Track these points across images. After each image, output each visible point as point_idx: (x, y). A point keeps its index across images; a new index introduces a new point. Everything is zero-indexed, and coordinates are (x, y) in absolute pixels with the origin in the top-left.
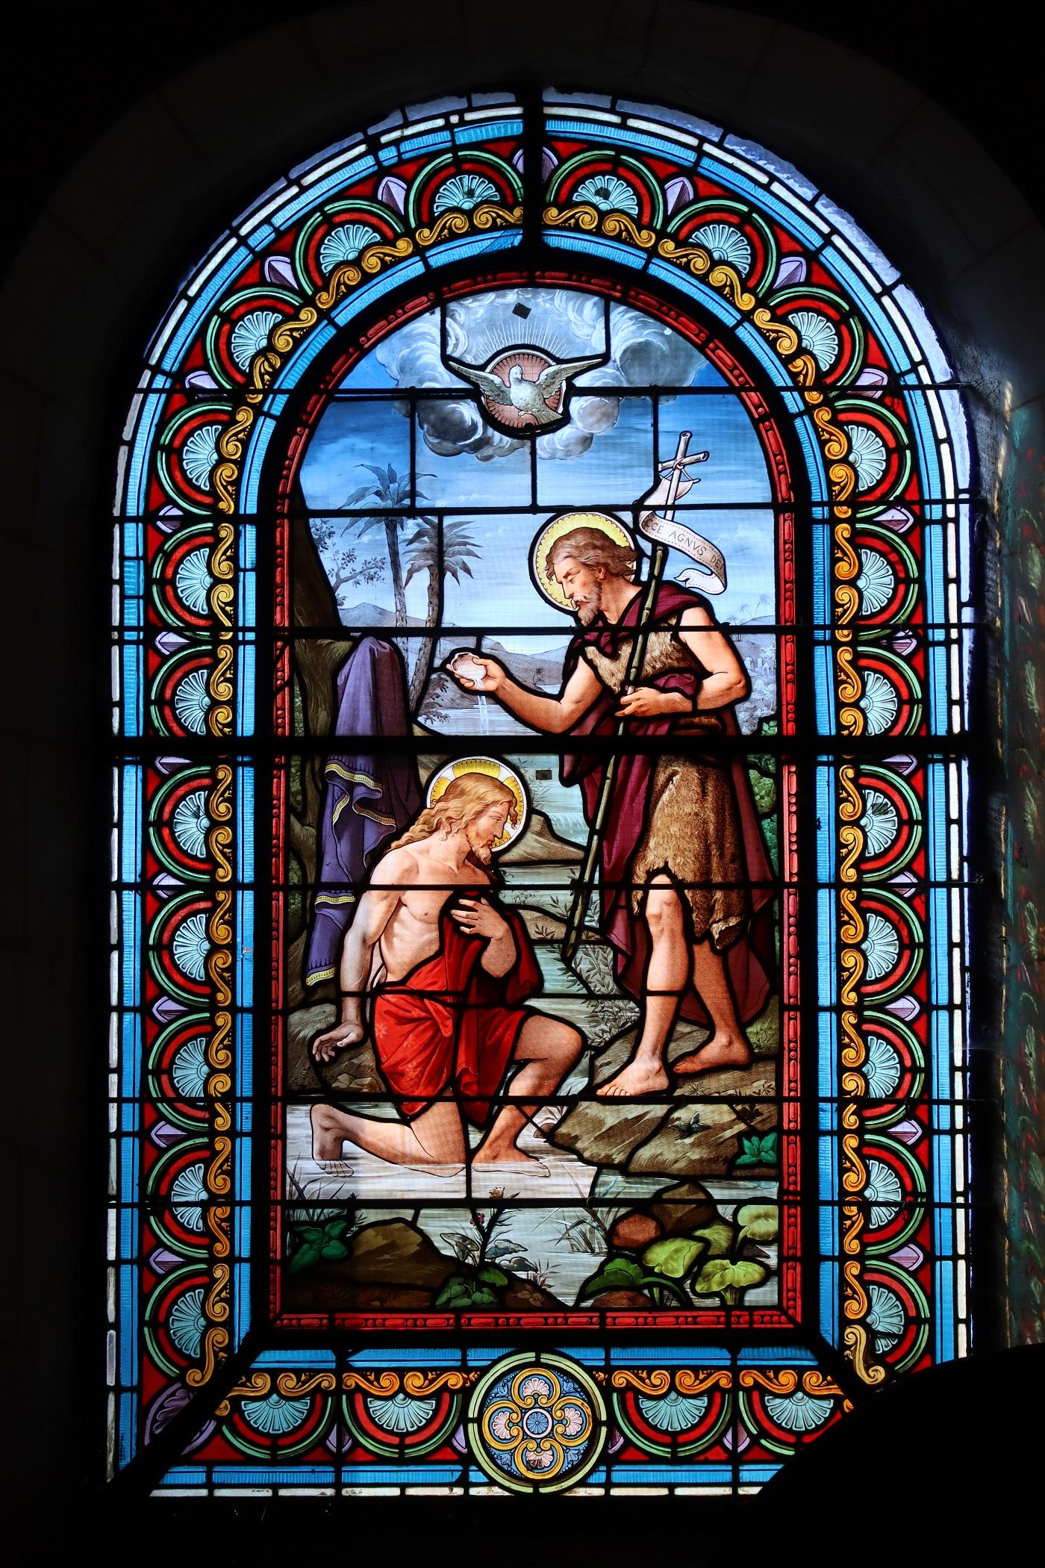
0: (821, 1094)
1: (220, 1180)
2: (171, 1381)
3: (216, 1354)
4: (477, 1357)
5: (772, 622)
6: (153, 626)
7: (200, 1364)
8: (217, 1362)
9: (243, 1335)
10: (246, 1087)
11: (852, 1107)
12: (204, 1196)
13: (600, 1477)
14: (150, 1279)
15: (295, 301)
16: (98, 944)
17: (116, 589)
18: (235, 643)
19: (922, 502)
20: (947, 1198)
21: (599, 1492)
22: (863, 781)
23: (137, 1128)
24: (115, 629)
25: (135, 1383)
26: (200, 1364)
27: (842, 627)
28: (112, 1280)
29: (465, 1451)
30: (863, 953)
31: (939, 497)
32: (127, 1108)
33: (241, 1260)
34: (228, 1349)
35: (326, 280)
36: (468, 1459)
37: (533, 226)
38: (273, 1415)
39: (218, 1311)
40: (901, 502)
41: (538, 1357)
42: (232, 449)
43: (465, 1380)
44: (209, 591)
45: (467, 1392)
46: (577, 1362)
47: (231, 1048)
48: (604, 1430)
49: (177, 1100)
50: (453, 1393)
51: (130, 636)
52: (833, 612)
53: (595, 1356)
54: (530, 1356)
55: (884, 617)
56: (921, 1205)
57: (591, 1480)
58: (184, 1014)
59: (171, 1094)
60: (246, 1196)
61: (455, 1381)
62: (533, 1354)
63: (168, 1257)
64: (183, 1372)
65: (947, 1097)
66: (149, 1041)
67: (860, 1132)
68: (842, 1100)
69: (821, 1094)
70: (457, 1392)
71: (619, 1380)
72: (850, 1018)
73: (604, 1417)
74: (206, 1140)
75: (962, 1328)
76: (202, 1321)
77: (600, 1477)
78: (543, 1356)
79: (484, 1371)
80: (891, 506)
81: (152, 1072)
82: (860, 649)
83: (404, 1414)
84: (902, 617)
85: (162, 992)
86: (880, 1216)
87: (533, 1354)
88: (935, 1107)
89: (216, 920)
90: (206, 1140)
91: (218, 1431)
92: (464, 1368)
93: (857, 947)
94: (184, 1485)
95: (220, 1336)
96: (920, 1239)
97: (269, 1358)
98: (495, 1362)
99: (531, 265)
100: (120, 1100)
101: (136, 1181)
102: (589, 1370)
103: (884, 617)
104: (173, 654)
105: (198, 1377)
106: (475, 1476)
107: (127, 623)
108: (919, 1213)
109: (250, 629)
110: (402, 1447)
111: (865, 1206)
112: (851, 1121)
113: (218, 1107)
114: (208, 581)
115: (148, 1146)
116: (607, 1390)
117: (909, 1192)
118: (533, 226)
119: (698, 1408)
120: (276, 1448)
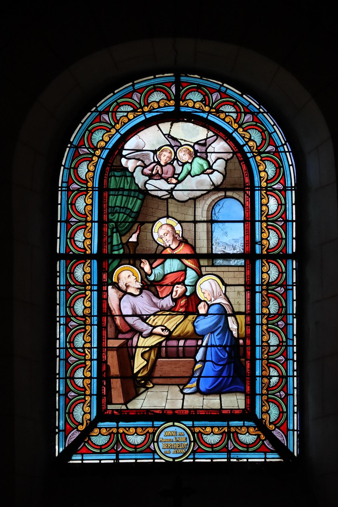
0: (257, 313)
1: (88, 338)
2: (74, 429)
3: (87, 421)
4: (157, 423)
5: (243, 283)
6: (68, 285)
7: (82, 424)
8: (87, 424)
9: (94, 418)
10: (95, 312)
11: (266, 317)
12: (83, 377)
13: (191, 456)
14: (68, 330)
15: (110, 127)
16: (53, 304)
17: (58, 324)
18: (91, 290)
19: (287, 285)
20: (291, 374)
21: (192, 461)
22: (269, 295)
23: (64, 393)
24: (60, 187)
25: (64, 429)
26: (82, 424)
27: (264, 285)
28: (58, 382)
29: (153, 449)
30: (268, 241)
31: (292, 375)
32: (62, 350)
33: (94, 360)
34: (90, 420)
35: (118, 121)
36: (154, 452)
37: (177, 106)
38: (101, 440)
39: (87, 409)
40: (281, 286)
41: (174, 424)
42: (92, 168)
43: (154, 430)
44: (86, 173)
45: (154, 433)
46: (185, 425)
47: (90, 406)
48: (192, 443)
49: (76, 316)
50: (150, 433)
51: (62, 288)
52: (262, 281)
53: (190, 423)
54: (171, 424)
55: (276, 282)
56: (284, 346)
57: (189, 457)
58: (77, 291)
59: (74, 315)
60: (96, 314)
61: (151, 430)
62: (172, 423)
63: (73, 394)
64: (77, 426)
65: (292, 375)
66: (69, 196)
67: (267, 324)
68: (262, 314)
69: (257, 313)
70: (151, 433)
71: (197, 430)
72: (265, 293)
73: (192, 440)
74: (84, 326)
75: (295, 415)
76: (83, 273)
77: (191, 456)
78: (175, 423)
79: (159, 427)
80: (279, 286)
81: (68, 342)
82: (269, 326)
83: (136, 440)
84: (281, 282)
85: (71, 390)
86: (272, 349)
87: (172, 423)
88: (288, 316)
89: (85, 406)
90: (84, 326)
91: (84, 445)
92: (153, 427)
93: (266, 239)
94: (76, 459)
95: (88, 416)
96: (283, 319)
97: (100, 424)
98: (162, 425)
99: (175, 117)
100: (60, 348)
101: (65, 266)
102: (188, 427)
103: (276, 282)
104: (73, 328)
105: (81, 428)
106: (156, 456)
107: (62, 220)
108: (283, 348)
109: (97, 188)
110: (136, 448)
111: (269, 346)
112: (265, 321)
113: (87, 318)
114: (83, 413)
115: (67, 328)
116: (193, 433)
117: (281, 342)
118: (177, 106)
119: (223, 108)
120: (101, 449)
